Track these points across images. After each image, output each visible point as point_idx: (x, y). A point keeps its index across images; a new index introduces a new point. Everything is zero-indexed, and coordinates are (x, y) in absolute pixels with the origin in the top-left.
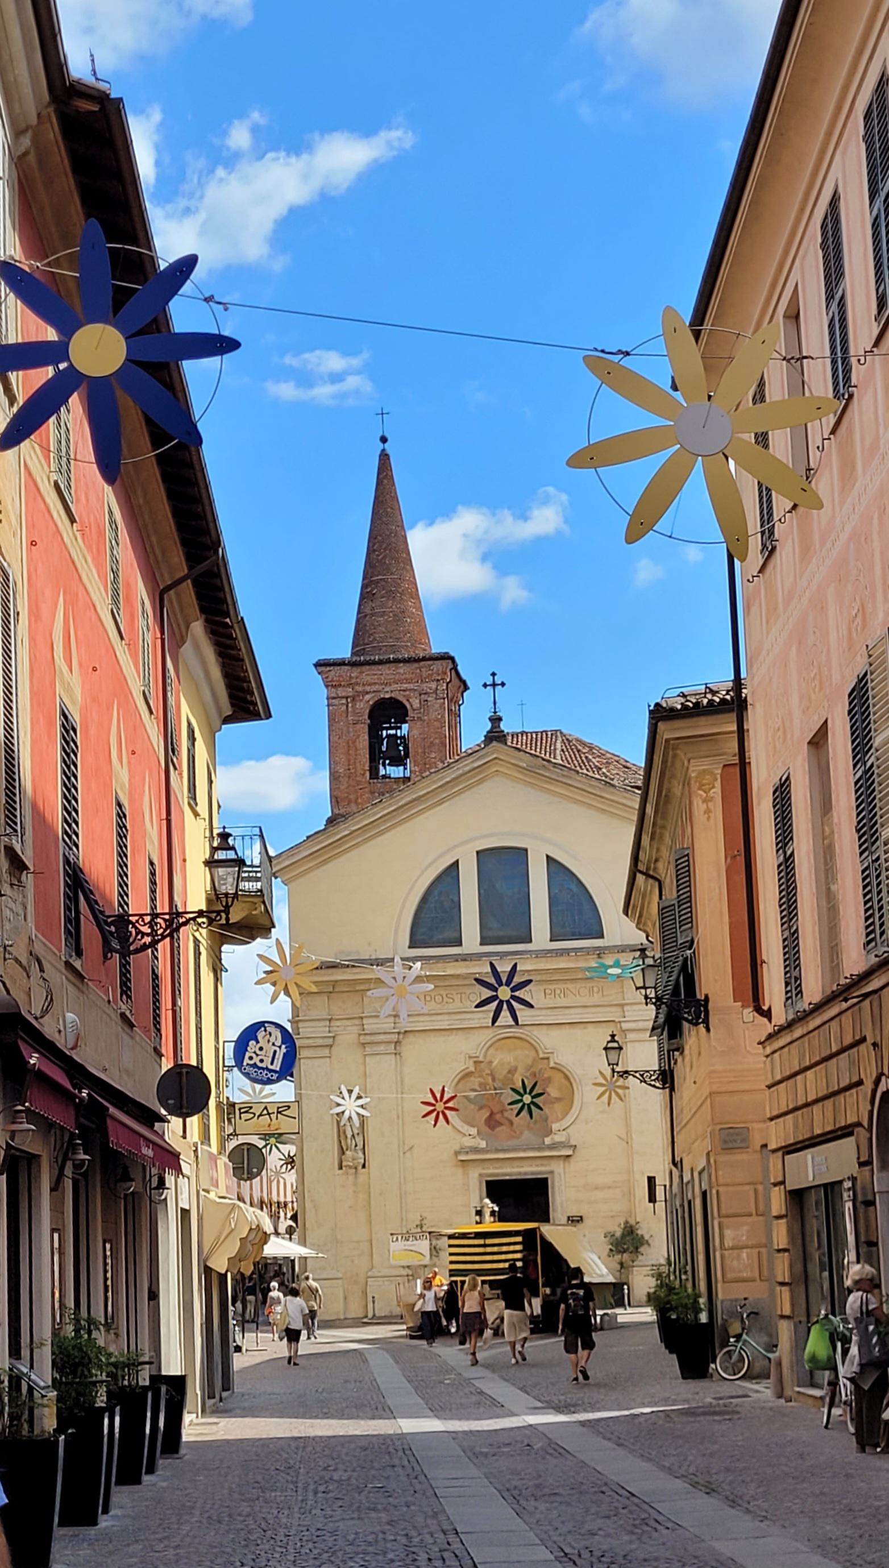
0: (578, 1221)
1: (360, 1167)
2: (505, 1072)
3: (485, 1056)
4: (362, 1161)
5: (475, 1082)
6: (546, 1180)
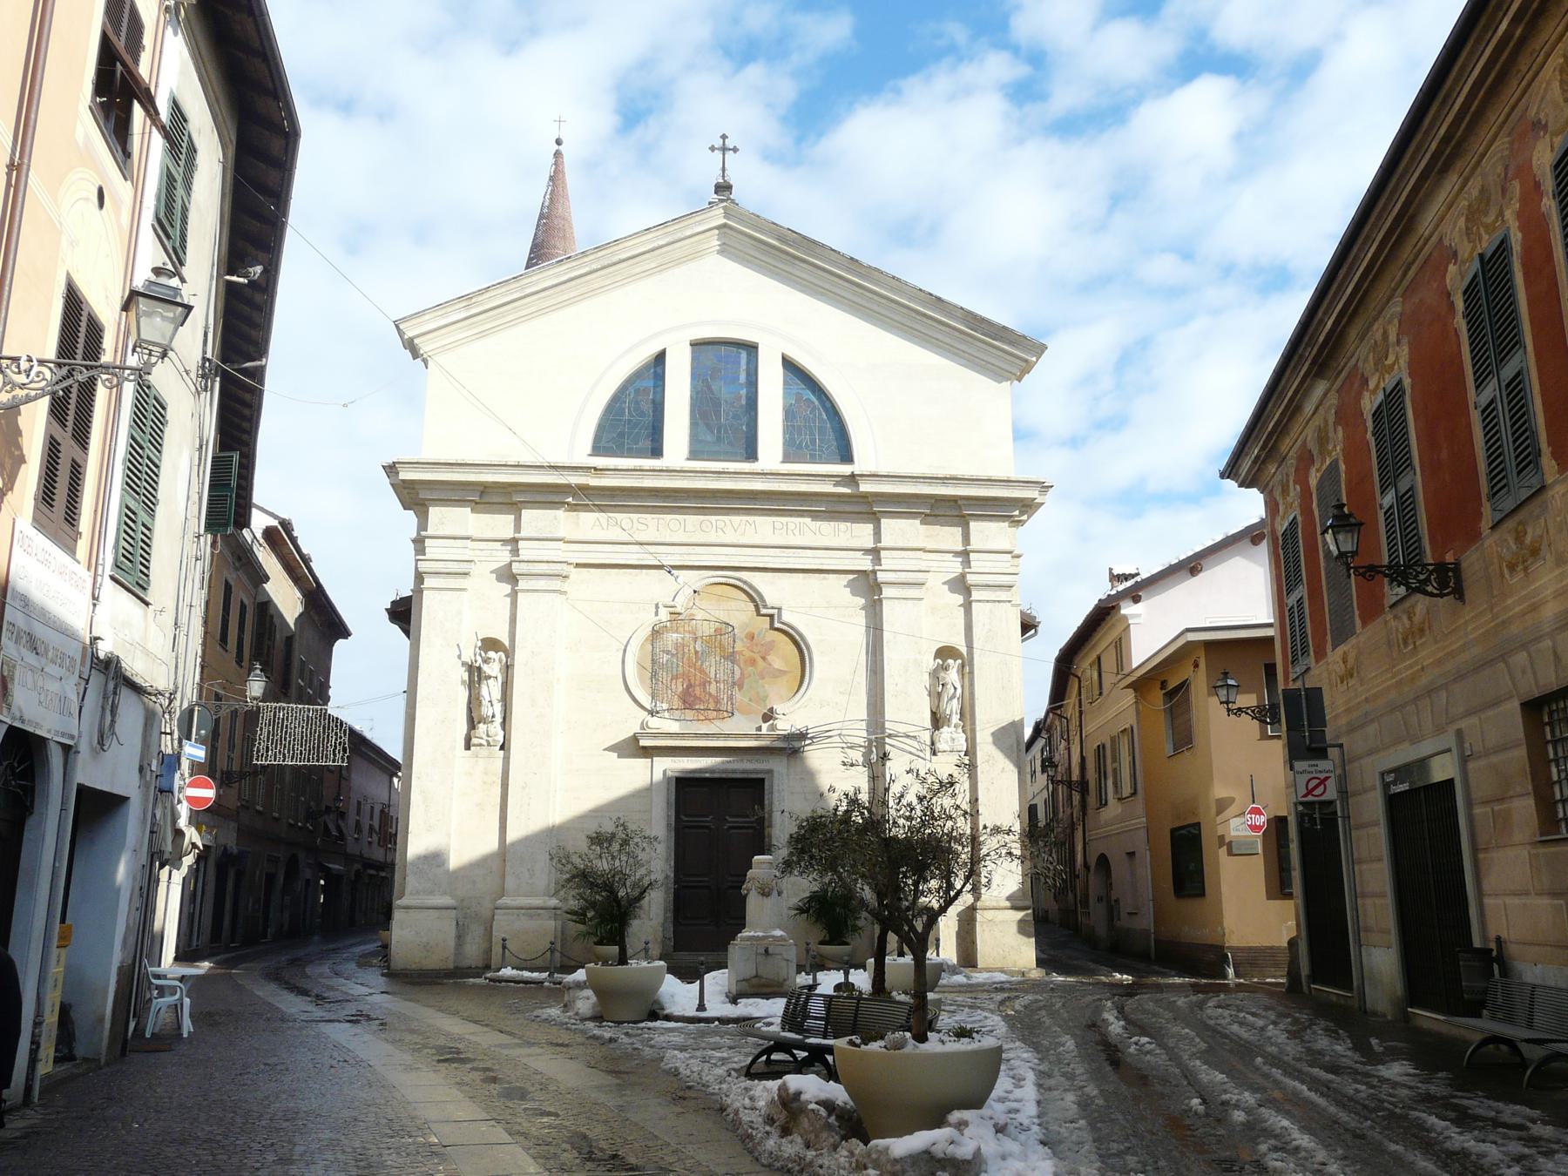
6: (763, 780)
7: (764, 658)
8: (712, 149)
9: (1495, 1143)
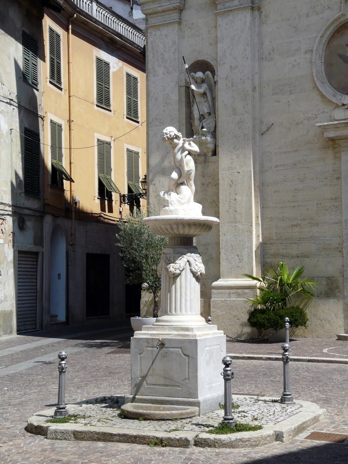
1: (210, 154)
4: (211, 146)
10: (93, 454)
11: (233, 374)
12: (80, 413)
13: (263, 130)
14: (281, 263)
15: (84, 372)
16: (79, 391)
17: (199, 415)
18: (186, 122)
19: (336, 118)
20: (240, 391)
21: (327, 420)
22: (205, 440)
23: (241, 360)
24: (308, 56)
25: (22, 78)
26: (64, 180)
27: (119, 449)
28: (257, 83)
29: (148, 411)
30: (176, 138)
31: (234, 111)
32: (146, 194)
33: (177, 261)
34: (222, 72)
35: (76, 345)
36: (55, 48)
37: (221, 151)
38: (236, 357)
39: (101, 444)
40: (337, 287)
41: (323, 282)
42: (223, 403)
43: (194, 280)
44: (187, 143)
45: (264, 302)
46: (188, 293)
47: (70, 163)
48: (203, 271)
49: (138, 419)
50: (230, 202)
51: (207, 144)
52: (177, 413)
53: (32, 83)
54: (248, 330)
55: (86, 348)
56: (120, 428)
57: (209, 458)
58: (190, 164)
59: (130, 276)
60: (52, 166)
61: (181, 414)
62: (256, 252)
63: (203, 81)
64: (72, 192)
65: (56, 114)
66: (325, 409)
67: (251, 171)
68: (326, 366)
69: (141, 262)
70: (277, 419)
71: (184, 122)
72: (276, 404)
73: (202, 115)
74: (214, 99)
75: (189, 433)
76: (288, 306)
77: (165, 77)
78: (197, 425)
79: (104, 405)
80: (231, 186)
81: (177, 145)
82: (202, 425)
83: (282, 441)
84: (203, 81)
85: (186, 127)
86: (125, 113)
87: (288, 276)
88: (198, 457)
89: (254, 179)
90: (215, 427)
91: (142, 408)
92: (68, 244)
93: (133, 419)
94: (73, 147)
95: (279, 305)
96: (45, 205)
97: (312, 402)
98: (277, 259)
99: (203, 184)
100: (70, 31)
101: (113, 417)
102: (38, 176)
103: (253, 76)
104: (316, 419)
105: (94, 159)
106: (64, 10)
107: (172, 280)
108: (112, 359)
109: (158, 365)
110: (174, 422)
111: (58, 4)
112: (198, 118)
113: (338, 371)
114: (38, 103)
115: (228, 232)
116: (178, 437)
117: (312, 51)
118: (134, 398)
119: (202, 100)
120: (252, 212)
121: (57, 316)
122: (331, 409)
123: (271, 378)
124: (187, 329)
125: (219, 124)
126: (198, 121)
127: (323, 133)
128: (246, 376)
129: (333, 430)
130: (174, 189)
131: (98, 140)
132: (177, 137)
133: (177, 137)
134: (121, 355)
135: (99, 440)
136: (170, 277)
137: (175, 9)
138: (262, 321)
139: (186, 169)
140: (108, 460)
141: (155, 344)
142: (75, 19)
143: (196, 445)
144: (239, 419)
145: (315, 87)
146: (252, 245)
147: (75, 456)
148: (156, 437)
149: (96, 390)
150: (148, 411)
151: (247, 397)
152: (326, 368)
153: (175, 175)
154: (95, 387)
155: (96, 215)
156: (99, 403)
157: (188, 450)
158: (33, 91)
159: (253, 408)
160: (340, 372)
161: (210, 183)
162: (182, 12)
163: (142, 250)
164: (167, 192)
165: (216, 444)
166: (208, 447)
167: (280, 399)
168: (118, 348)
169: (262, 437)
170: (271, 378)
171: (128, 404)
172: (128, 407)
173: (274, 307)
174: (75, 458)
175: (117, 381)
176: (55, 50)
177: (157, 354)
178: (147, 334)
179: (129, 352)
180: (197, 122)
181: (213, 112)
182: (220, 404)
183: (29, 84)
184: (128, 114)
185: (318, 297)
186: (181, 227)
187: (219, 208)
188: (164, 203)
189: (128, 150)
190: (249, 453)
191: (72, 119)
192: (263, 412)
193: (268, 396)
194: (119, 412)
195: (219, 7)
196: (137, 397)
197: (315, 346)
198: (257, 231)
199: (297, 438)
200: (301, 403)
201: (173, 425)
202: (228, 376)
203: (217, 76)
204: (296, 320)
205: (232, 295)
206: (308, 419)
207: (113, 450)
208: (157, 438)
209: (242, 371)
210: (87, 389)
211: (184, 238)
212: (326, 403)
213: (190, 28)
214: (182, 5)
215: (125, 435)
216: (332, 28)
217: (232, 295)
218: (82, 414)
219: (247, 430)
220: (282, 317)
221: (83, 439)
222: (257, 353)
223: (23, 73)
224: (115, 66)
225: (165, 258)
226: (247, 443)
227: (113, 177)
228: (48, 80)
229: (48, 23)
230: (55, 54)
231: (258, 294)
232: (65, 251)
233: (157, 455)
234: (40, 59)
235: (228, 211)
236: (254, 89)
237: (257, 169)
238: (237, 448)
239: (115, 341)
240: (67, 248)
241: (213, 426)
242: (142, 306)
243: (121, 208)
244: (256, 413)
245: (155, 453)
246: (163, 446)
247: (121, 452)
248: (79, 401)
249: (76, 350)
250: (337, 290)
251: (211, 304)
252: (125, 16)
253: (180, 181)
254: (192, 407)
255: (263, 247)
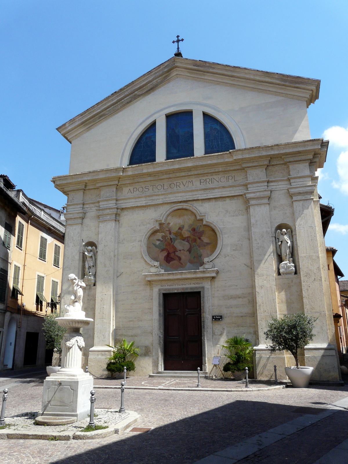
0: (219, 319)
1: (92, 285)
2: (177, 229)
3: (166, 220)
4: (93, 282)
5: (159, 235)
6: (199, 293)
7: (200, 238)
8: (178, 37)
9: (79, 181)
10: (17, 447)
11: (95, 399)
12: (12, 423)
13: (118, 275)
14: (124, 339)
15: (18, 398)
16: (14, 409)
17: (77, 422)
18: (82, 269)
19: (151, 272)
20: (99, 406)
21: (141, 421)
22: (79, 436)
23: (102, 389)
24: (139, 243)
25: (2, 244)
26: (18, 295)
27: (32, 443)
28: (116, 254)
29: (50, 421)
30: (75, 280)
31: (105, 266)
32: (59, 303)
33: (70, 341)
34: (100, 248)
35: (16, 382)
36: (21, 231)
37: (97, 284)
38: (99, 387)
39: (22, 441)
40: (150, 351)
41: (143, 349)
42: (89, 414)
43: (79, 350)
44: (80, 282)
45: (115, 359)
46: (75, 356)
47: (23, 286)
48: (84, 346)
49: (44, 425)
50: (101, 308)
51: (91, 280)
52: (65, 421)
53: (7, 246)
54: (106, 373)
55: (21, 383)
56: (34, 431)
57: (80, 446)
58: (80, 292)
59: (48, 345)
60: (13, 287)
61: (67, 421)
62: (112, 333)
63: (91, 251)
64: (22, 301)
65: (17, 262)
66: (140, 415)
67: (111, 294)
68: (143, 391)
69: (54, 338)
70: (116, 422)
71: (81, 269)
72: (117, 413)
73: (90, 267)
74: (96, 259)
75: (70, 433)
76: (126, 361)
77: (71, 250)
78: (75, 427)
79: (26, 417)
80: (101, 301)
81: (75, 283)
82: (78, 427)
83: (118, 434)
84: (91, 251)
85: (82, 272)
86: (53, 263)
87: (127, 346)
88: (74, 446)
89: (113, 298)
90: (85, 428)
91: (47, 419)
92: (17, 327)
93: (41, 425)
94: (24, 278)
95: (122, 360)
96: (7, 307)
97: (135, 411)
98: (122, 337)
99: (88, 300)
100: (29, 223)
101: (31, 424)
102: (5, 292)
103: (114, 250)
104: (135, 421)
105: (35, 285)
106: (27, 214)
107: (68, 350)
108: (34, 389)
109: (58, 395)
110: (63, 426)
111: (23, 210)
112: (88, 268)
113: (148, 393)
114: (9, 256)
115: (99, 323)
116: (64, 435)
117: (141, 241)
118: (43, 413)
119: (90, 259)
120: (111, 314)
121: (7, 365)
122: (143, 414)
123: (116, 399)
124: (74, 376)
125: (98, 272)
126: (88, 269)
127: (145, 278)
128: (103, 398)
129: (143, 426)
130: (72, 304)
131: (38, 275)
132: (75, 279)
133: (75, 279)
134: (39, 387)
135: (21, 438)
136: (67, 348)
137: (80, 218)
138: (113, 368)
139: (79, 294)
140: (25, 450)
141: (57, 383)
142: (33, 218)
143: (73, 439)
144: (97, 423)
145: (142, 257)
146: (110, 330)
147: (6, 449)
148: (53, 436)
149: (23, 408)
150: (50, 421)
151: (102, 410)
152: (143, 392)
153: (73, 297)
154: (23, 406)
155: (33, 312)
156: (24, 416)
157: (69, 442)
158: (7, 250)
159: (105, 416)
160: (149, 394)
161: (91, 299)
162: (84, 219)
163: (55, 332)
164: (69, 305)
165: (84, 437)
166: (80, 439)
167: (119, 410)
168: (39, 383)
169: (108, 432)
170: (116, 399)
171: (39, 416)
172: (39, 419)
173: (120, 361)
174: (6, 450)
175: (36, 402)
176: (21, 232)
177: (57, 389)
178: (53, 378)
179: (43, 385)
180: (87, 270)
181: (95, 265)
182: (88, 415)
183: (6, 247)
184: (54, 263)
185: (141, 356)
186: (74, 323)
187: (95, 311)
188: (67, 311)
189: (53, 281)
190: (100, 441)
191: (25, 265)
192: (110, 418)
193: (113, 409)
194: (34, 421)
195: (100, 218)
196: (44, 412)
197: (138, 381)
198: (113, 323)
199: (125, 431)
200: (129, 412)
201: (62, 428)
202: (93, 400)
203: (98, 249)
204: (130, 368)
205: (99, 355)
206: (131, 421)
207: (28, 444)
208: (53, 436)
209: (102, 395)
210: (18, 408)
211: (75, 329)
212: (141, 411)
213: (86, 226)
214: (83, 216)
215: (35, 435)
216: (150, 232)
217: (99, 355)
218: (13, 423)
219: (101, 429)
220: (123, 366)
221: (12, 438)
222: (110, 385)
223: (3, 242)
224: (50, 240)
225: (65, 339)
226: (100, 436)
227: (44, 294)
228: (16, 245)
229: (19, 219)
230: (21, 233)
231: (112, 355)
232: (15, 330)
233: (52, 446)
234: (13, 235)
235: (99, 313)
236: (115, 256)
237: (115, 293)
238: (95, 439)
239: (38, 379)
240: (16, 329)
241: (83, 428)
242: (53, 360)
243: (47, 309)
244: (106, 419)
245: (51, 445)
246: (56, 440)
247: (32, 445)
248: (13, 415)
249: (16, 384)
250: (150, 353)
251: (89, 359)
252: (57, 218)
253: (75, 300)
254: (73, 417)
255: (115, 331)
